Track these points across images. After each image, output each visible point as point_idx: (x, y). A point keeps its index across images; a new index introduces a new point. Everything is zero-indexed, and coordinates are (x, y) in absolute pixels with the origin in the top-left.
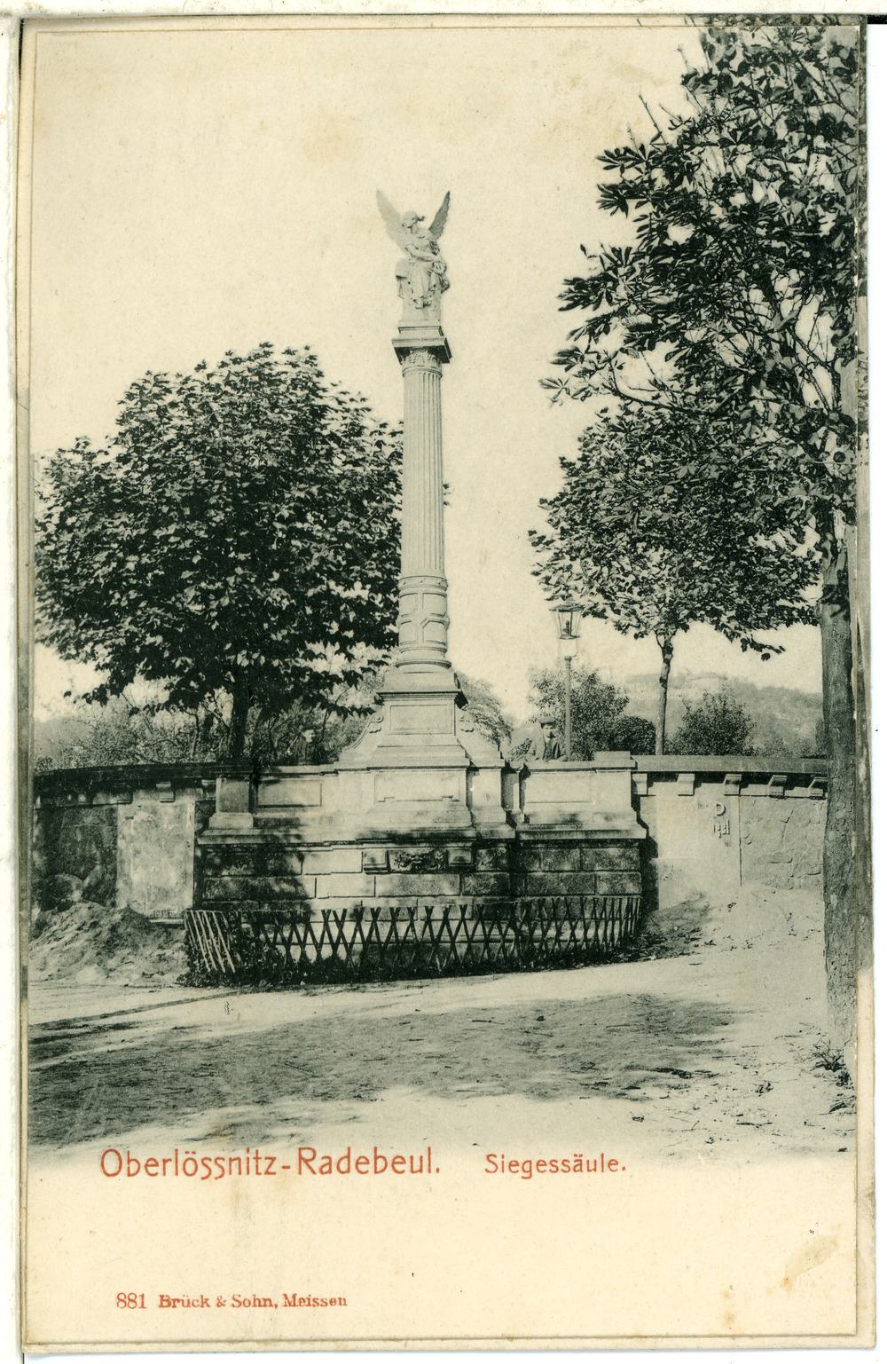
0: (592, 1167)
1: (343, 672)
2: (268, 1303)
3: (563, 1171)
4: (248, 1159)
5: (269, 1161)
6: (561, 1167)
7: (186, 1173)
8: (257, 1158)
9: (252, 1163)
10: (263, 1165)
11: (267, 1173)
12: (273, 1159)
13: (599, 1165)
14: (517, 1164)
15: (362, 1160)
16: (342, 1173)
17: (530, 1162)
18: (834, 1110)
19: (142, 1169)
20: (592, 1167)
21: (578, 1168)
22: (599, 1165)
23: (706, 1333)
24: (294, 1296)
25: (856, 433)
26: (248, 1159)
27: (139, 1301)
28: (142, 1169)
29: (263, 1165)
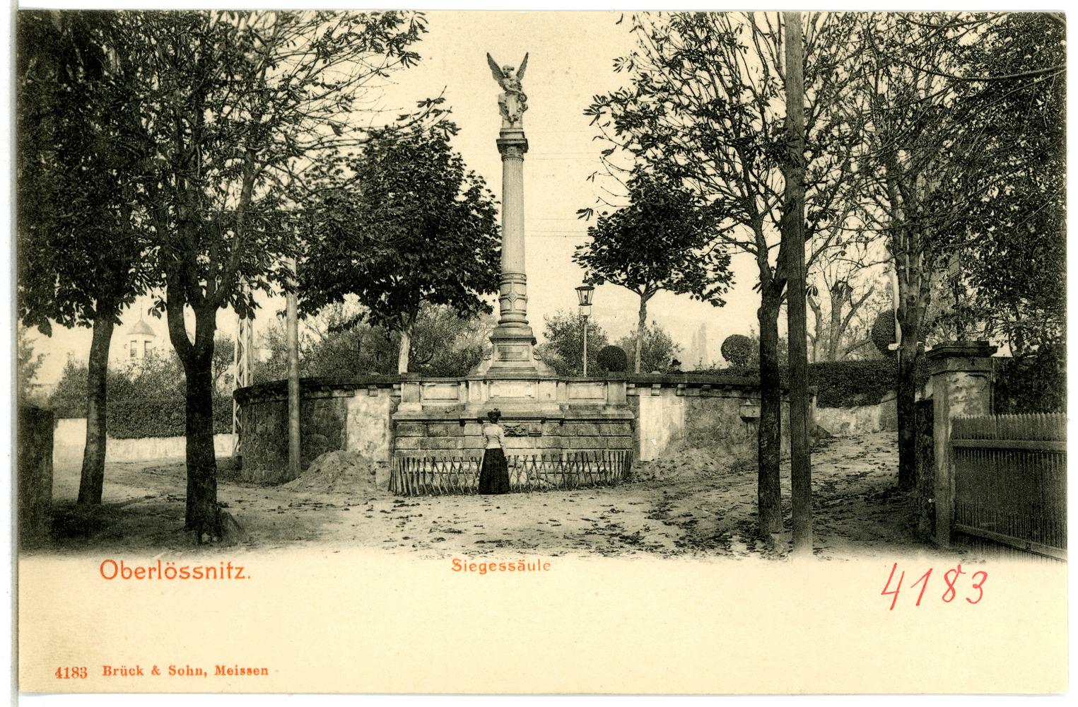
0: (531, 568)
1: (32, 349)
2: (265, 672)
3: (194, 577)
4: (222, 569)
5: (238, 570)
6: (192, 574)
7: (123, 575)
8: (229, 568)
9: (225, 572)
10: (234, 572)
11: (237, 577)
12: (241, 569)
13: (537, 567)
14: (476, 566)
15: (140, 570)
16: (127, 578)
17: (485, 565)
18: (460, 532)
19: (133, 574)
20: (531, 568)
21: (521, 569)
22: (537, 567)
23: (578, 691)
24: (223, 667)
25: (659, 283)
26: (222, 569)
27: (70, 673)
28: (133, 574)
29: (234, 572)
